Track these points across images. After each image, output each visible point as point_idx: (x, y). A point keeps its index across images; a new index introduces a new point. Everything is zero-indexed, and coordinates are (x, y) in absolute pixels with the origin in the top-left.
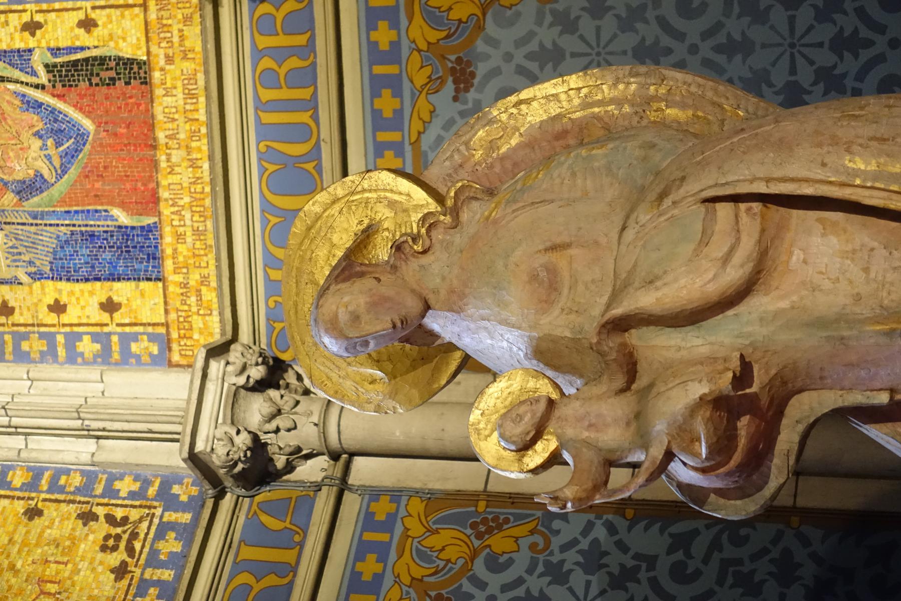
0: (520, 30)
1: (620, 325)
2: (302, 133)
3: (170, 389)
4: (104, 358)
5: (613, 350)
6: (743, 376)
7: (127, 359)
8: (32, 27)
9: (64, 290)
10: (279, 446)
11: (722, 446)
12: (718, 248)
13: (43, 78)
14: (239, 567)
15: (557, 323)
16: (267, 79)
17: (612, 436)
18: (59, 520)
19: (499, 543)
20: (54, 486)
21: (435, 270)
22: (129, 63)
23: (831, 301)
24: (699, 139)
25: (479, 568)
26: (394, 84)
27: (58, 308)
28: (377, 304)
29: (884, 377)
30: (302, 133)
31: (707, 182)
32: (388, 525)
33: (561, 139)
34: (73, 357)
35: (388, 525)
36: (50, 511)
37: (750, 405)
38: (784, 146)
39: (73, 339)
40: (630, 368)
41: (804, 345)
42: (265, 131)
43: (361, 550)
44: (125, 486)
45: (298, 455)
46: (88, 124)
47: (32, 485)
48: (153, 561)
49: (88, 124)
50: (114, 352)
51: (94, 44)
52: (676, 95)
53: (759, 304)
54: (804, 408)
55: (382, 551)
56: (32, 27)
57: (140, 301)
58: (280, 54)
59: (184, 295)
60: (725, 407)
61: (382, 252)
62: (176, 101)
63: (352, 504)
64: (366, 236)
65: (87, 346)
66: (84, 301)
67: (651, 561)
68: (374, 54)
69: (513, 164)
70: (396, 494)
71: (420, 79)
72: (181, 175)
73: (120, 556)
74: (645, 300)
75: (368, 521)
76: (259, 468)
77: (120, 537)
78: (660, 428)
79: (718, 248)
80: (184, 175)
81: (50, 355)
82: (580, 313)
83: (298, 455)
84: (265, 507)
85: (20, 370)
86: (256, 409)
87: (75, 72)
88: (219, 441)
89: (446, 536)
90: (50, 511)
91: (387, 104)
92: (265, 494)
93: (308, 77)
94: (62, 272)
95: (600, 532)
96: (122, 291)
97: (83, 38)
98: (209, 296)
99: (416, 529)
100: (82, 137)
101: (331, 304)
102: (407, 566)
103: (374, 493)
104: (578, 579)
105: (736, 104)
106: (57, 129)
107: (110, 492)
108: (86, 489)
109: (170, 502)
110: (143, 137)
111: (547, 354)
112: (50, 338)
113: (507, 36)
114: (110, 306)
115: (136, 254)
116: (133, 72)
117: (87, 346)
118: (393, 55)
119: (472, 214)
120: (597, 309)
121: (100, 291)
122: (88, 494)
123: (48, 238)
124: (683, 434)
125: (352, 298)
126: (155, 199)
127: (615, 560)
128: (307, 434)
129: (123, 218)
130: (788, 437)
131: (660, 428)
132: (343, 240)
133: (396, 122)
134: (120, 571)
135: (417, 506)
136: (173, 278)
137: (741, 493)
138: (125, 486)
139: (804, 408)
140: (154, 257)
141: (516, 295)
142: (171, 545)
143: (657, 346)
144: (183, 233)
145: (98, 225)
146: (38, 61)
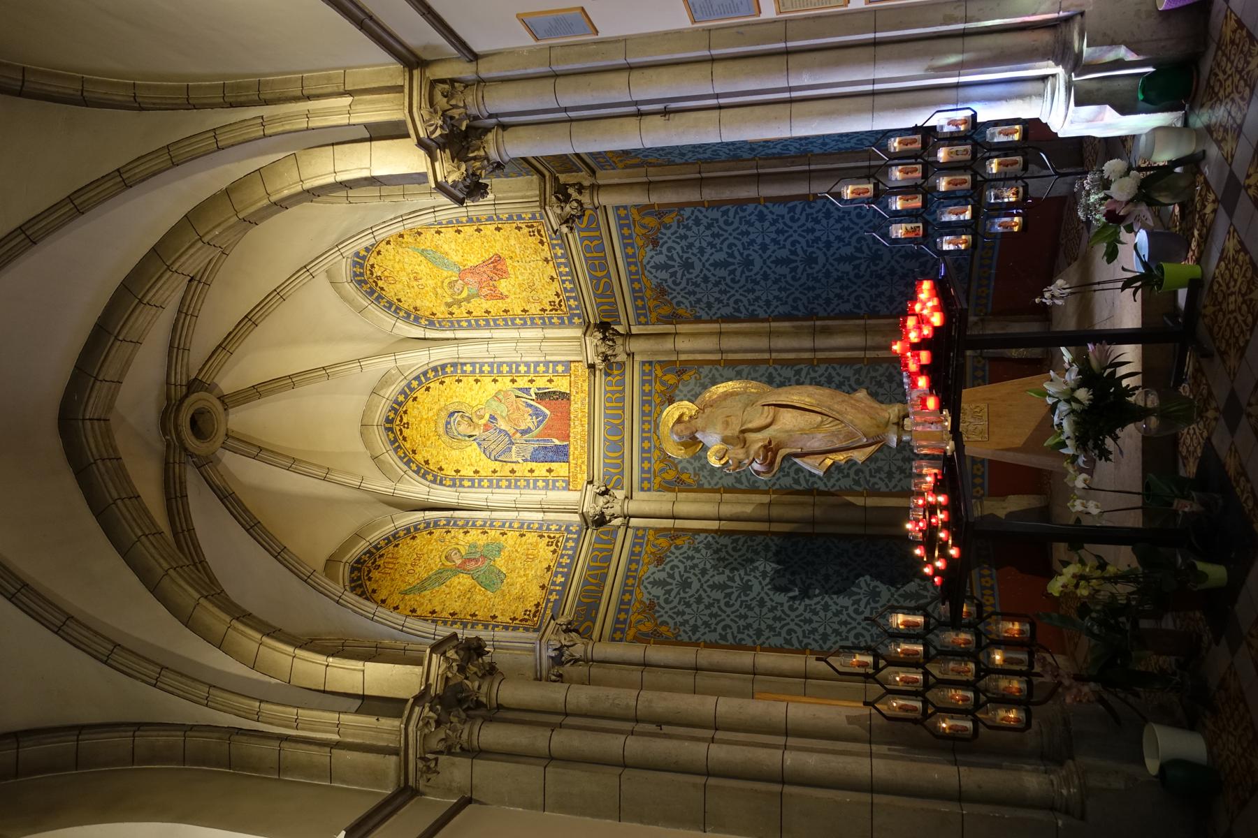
0: (689, 388)
1: (743, 432)
2: (619, 417)
3: (572, 497)
4: (546, 488)
5: (741, 438)
6: (770, 442)
7: (554, 488)
8: (531, 381)
9: (534, 465)
10: (608, 512)
11: (765, 458)
12: (765, 414)
13: (534, 397)
14: (594, 550)
15: (728, 433)
16: (609, 400)
17: (741, 456)
18: (531, 537)
19: (678, 542)
20: (528, 527)
21: (699, 423)
22: (563, 393)
23: (788, 427)
24: (760, 395)
25: (672, 548)
26: (649, 402)
27: (531, 471)
28: (687, 428)
29: (800, 445)
30: (619, 417)
31: (763, 401)
32: (643, 537)
33: (726, 396)
34: (535, 487)
35: (643, 537)
36: (528, 535)
37: (771, 450)
38: (780, 394)
39: (536, 481)
40: (745, 442)
41: (783, 436)
42: (606, 416)
43: (634, 545)
44: (553, 527)
45: (614, 516)
46: (548, 412)
47: (521, 527)
48: (565, 548)
49: (548, 412)
50: (549, 485)
51: (552, 387)
52: (753, 387)
53: (773, 427)
54: (782, 452)
55: (641, 545)
56: (531, 381)
57: (560, 469)
58: (613, 392)
59: (576, 466)
60: (766, 448)
61: (686, 418)
62: (578, 406)
63: (630, 532)
64: (681, 416)
65: (541, 484)
66: (541, 469)
67: (726, 546)
68: (643, 393)
69: (715, 401)
70: (645, 529)
71: (658, 401)
72: (578, 429)
73: (554, 547)
74: (750, 426)
75: (636, 536)
76: (600, 521)
77: (552, 542)
78: (752, 452)
79: (765, 414)
80: (579, 429)
81: (528, 486)
82: (734, 430)
83: (614, 516)
84: (602, 533)
85: (518, 491)
86: (601, 500)
87: (543, 396)
88: (591, 508)
89: (661, 540)
90: (528, 535)
91: (647, 408)
92: (601, 529)
93: (623, 399)
94: (533, 460)
95: (710, 539)
96: (554, 466)
97: (549, 385)
98: (584, 467)
99: (652, 538)
100: (545, 416)
101: (675, 428)
102: (650, 549)
103: (638, 529)
104: (704, 552)
105: (767, 388)
106: (537, 413)
107: (548, 529)
108: (540, 528)
109: (570, 532)
110: (566, 417)
111: (725, 440)
112: (528, 481)
113: (685, 390)
114: (550, 471)
115: (561, 454)
116: (565, 396)
117: (541, 484)
118: (650, 394)
119: (708, 411)
120: (738, 429)
121: (547, 465)
122: (541, 530)
123: (530, 448)
124: (757, 454)
125: (680, 427)
126: (569, 436)
127: (715, 546)
128: (617, 509)
129: (557, 442)
130: (779, 459)
131: (752, 452)
132: (676, 416)
133: (649, 414)
134: (554, 552)
135: (651, 532)
136: (572, 462)
137: (768, 472)
138: (553, 527)
139: (782, 452)
140: (567, 455)
141: (719, 427)
142: (571, 544)
143: (751, 436)
144: (577, 448)
145: (549, 444)
146: (532, 392)
